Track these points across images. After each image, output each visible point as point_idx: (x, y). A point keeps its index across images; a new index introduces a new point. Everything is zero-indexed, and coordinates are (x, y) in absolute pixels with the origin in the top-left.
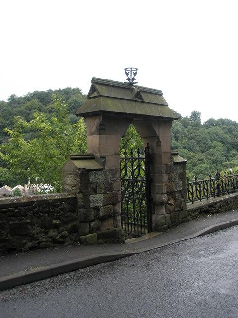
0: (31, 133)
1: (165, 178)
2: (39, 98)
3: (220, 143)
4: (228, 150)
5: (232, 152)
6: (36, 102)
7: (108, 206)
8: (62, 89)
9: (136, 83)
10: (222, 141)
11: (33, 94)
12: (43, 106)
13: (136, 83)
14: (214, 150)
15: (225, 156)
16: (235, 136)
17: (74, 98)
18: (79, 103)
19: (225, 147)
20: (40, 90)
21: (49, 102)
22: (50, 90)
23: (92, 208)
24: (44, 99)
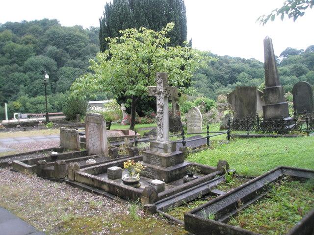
0: (6, 66)
1: (236, 227)
2: (13, 29)
3: (205, 75)
4: (212, 82)
5: (216, 84)
6: (10, 33)
7: (117, 132)
8: (39, 19)
9: (110, 3)
10: (206, 73)
11: (5, 25)
12: (17, 37)
13: (110, 3)
14: (200, 82)
15: (210, 87)
16: (217, 68)
17: (52, 29)
18: (58, 34)
19: (209, 79)
20: (13, 21)
21: (25, 33)
22: (25, 21)
23: (222, 73)
24: (18, 30)
